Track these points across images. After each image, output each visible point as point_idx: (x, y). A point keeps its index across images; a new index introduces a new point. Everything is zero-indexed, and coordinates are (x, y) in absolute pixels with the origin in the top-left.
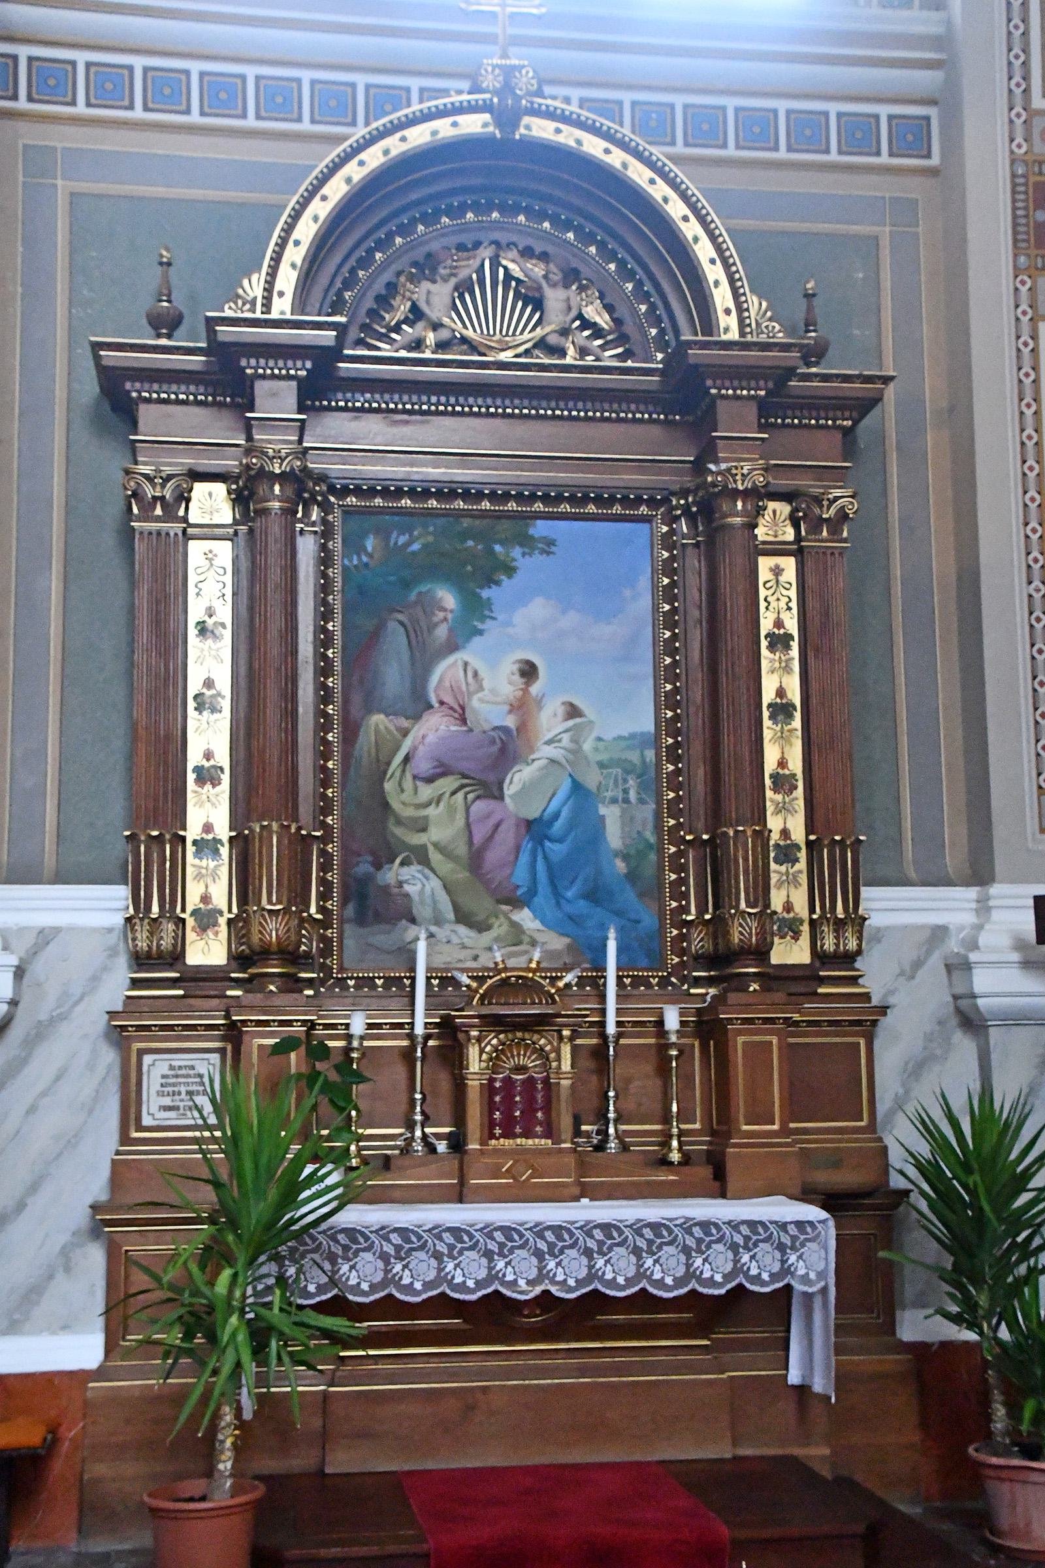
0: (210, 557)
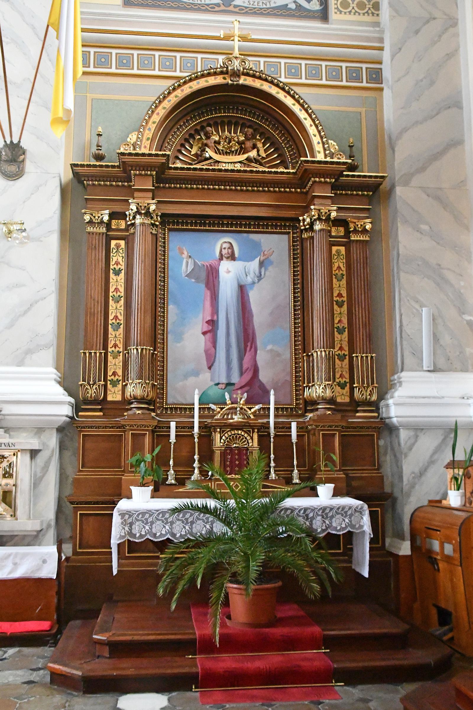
0: (118, 246)
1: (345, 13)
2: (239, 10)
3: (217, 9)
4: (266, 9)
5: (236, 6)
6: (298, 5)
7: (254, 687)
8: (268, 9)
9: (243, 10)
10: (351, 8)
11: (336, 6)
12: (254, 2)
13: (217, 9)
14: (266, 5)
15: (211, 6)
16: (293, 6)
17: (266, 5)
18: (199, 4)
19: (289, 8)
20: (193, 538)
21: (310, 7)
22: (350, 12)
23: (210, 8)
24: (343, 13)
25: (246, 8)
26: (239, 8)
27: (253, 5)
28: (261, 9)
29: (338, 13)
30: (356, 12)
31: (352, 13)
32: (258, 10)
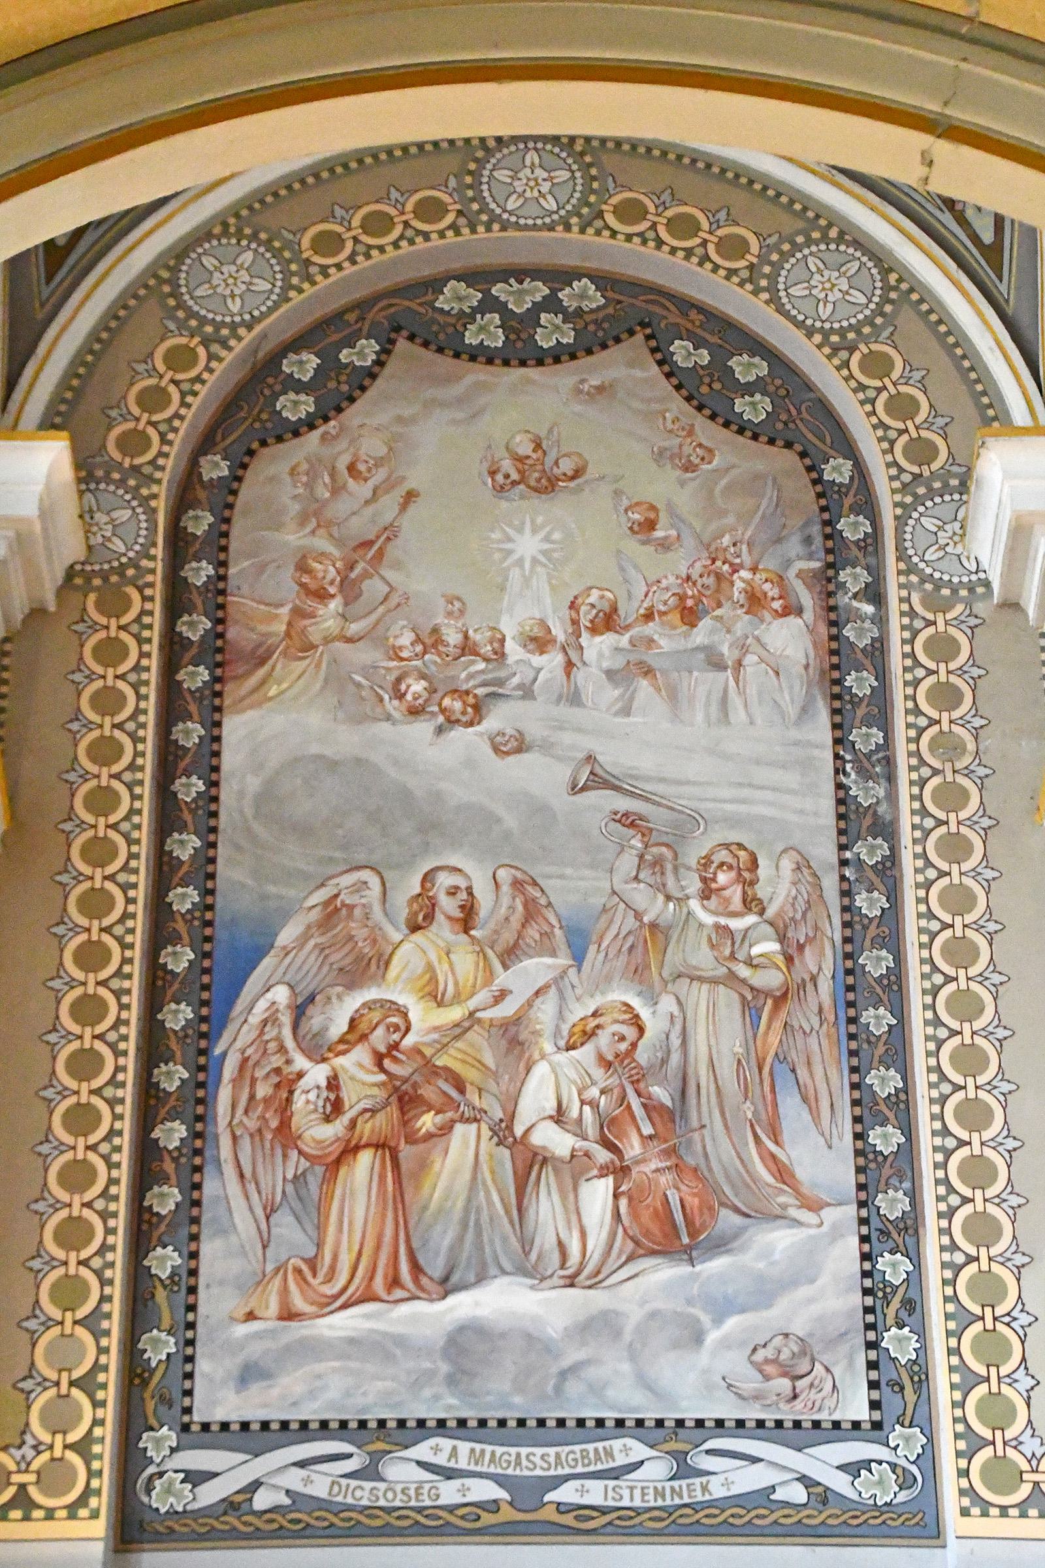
1: (1004, 1511)
3: (487, 1519)
4: (632, 1514)
24: (994, 1511)
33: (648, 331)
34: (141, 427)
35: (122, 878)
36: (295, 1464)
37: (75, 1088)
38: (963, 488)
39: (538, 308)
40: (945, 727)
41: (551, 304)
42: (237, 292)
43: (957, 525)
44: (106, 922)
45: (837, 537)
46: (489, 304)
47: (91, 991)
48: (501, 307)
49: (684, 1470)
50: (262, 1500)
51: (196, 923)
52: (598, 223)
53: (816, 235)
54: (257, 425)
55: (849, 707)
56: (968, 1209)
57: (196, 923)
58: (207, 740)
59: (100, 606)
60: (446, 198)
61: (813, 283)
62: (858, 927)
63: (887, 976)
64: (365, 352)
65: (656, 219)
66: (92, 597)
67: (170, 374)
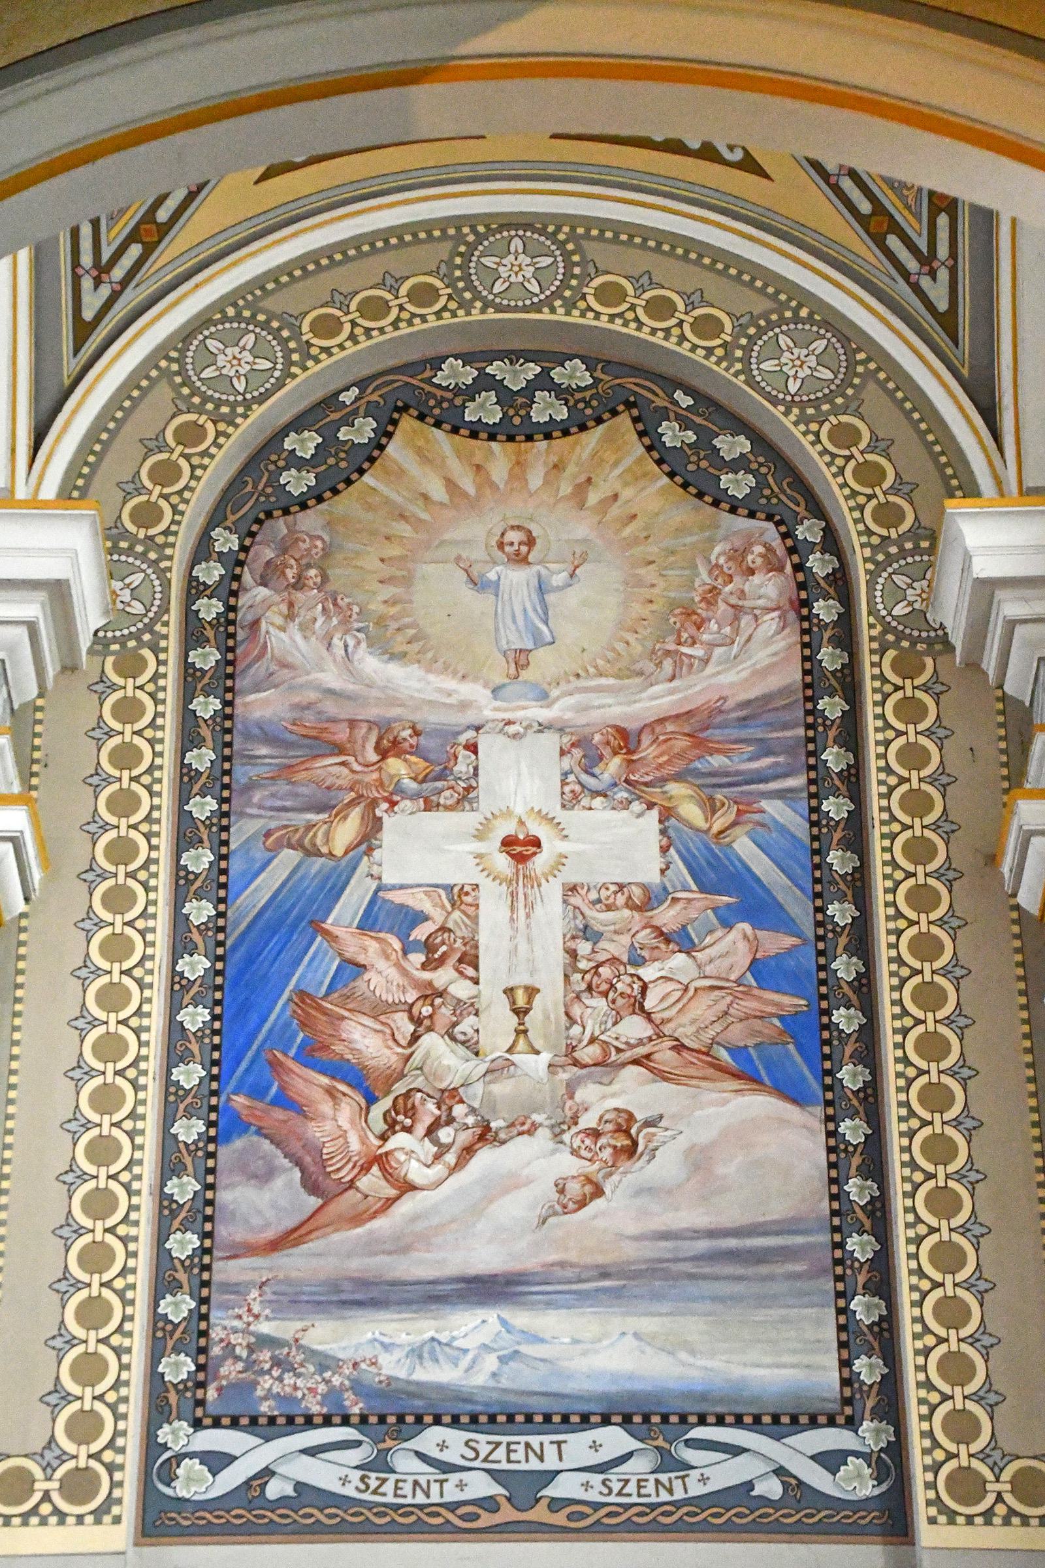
1: (970, 1520)
2: (569, 1517)
3: (486, 1520)
5: (556, 1504)
6: (794, 1482)
7: (654, 62)
8: (678, 1505)
9: (585, 1516)
10: (990, 1499)
11: (931, 1494)
12: (627, 1481)
13: (486, 1520)
14: (670, 1491)
15: (462, 1511)
16: (772, 1488)
17: (670, 1491)
18: (421, 1507)
19: (760, 1497)
20: (991, 674)
21: (838, 1485)
22: (988, 1515)
23: (461, 1517)
24: (960, 1520)
25: (596, 1506)
26: (568, 1510)
27: (620, 1494)
28: (653, 1507)
29: (942, 1519)
30: (1012, 1512)
31: (997, 1520)
32: (640, 1514)
33: (635, 412)
34: (153, 499)
35: (122, 1230)
36: (304, 1451)
37: (84, 1337)
38: (932, 550)
39: (531, 388)
40: (915, 784)
41: (543, 382)
42: (242, 371)
43: (925, 583)
44: (126, 965)
45: (837, 1088)
46: (485, 382)
47: (105, 1132)
48: (496, 385)
49: (668, 1463)
50: (275, 1489)
51: (200, 1153)
52: (582, 305)
53: (788, 314)
54: (262, 499)
55: (830, 935)
56: (927, 1131)
57: (214, 829)
58: (222, 664)
59: (119, 669)
60: (438, 284)
61: (783, 360)
62: (821, 729)
63: (878, 1324)
64: (363, 431)
65: (636, 301)
66: (110, 660)
67: (180, 448)
